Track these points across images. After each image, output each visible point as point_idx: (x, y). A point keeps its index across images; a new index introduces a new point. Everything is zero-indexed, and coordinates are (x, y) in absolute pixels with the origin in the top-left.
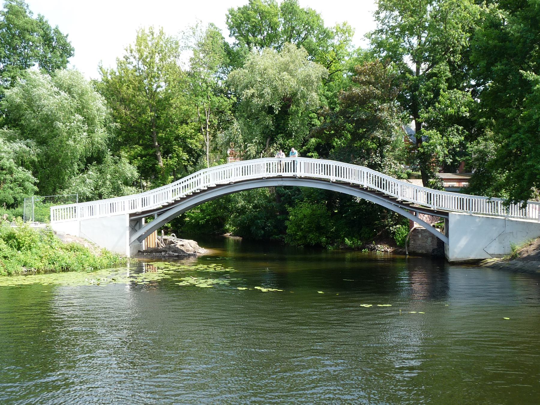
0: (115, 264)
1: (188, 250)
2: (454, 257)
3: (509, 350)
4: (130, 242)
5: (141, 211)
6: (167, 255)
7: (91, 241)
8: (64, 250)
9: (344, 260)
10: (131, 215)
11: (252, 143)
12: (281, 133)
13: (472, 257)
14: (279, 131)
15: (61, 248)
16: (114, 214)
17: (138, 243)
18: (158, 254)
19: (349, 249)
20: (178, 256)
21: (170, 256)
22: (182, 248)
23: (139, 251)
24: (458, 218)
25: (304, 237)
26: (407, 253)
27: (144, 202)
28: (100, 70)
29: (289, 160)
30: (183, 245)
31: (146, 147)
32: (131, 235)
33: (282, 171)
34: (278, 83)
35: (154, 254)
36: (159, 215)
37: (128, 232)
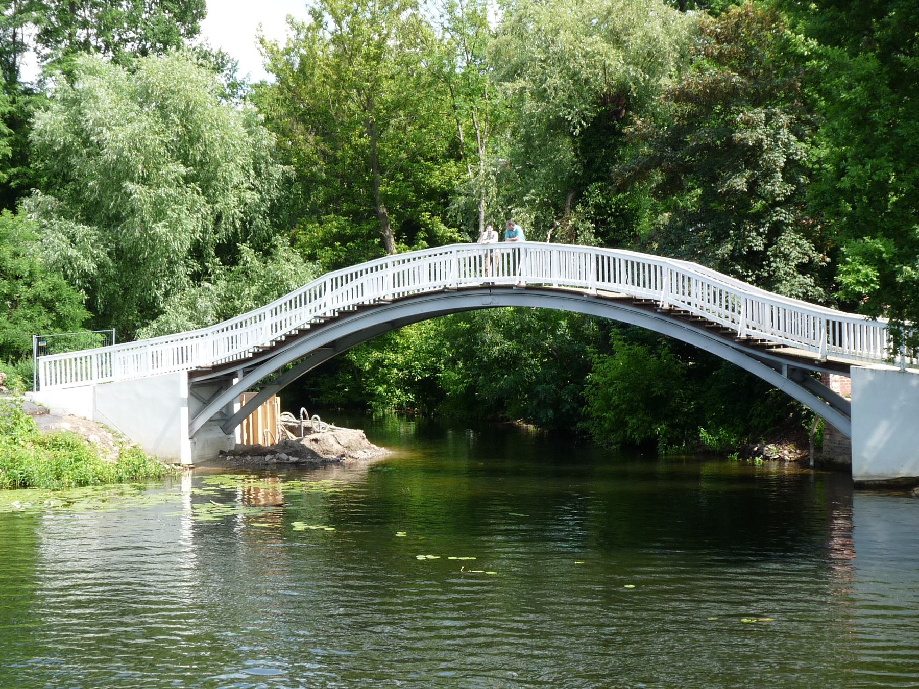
0: (139, 475)
1: (326, 452)
2: (862, 472)
3: (101, 589)
4: (190, 431)
5: (211, 365)
6: (275, 460)
7: (115, 429)
8: (38, 446)
9: (697, 477)
10: (192, 374)
11: (522, 205)
12: (597, 180)
13: (905, 471)
14: (594, 175)
15: (34, 442)
16: (160, 370)
17: (217, 433)
18: (257, 459)
19: (709, 454)
20: (296, 464)
21: (281, 465)
22: (314, 447)
23: (222, 452)
24: (870, 377)
25: (620, 424)
26: (812, 463)
27: (232, 341)
28: (261, 46)
29: (507, 247)
30: (316, 441)
31: (357, 217)
32: (193, 417)
33: (495, 273)
34: (578, 64)
35: (249, 458)
36: (246, 372)
37: (185, 412)
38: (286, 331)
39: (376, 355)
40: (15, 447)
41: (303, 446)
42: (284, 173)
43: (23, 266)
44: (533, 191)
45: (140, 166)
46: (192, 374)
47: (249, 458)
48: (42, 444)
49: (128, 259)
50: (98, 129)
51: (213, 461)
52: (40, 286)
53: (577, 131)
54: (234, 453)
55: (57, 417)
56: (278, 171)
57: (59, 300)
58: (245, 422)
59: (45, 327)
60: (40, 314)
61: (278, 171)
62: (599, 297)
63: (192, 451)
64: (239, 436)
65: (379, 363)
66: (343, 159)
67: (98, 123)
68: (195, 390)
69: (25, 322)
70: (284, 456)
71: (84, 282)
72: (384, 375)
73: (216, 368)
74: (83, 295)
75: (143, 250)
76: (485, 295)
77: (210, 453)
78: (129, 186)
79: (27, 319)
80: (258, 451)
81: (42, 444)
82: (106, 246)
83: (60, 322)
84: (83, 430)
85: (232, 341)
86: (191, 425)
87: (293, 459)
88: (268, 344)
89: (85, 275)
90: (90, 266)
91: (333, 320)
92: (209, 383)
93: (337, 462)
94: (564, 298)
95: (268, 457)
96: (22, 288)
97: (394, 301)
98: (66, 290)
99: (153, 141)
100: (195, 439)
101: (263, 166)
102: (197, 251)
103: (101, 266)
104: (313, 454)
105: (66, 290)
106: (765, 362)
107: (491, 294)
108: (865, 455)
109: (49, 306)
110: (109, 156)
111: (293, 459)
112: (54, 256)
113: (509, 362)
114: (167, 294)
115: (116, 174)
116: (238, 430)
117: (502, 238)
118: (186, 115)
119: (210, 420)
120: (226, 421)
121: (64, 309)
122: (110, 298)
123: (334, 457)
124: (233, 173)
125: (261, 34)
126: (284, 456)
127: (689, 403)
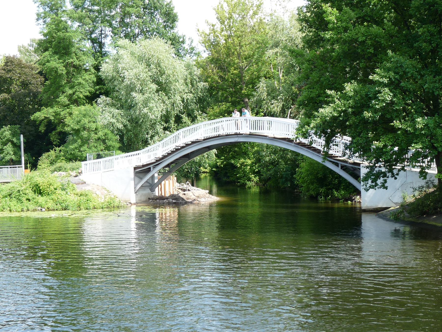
0: (111, 207)
5: (141, 165)
10: (135, 168)
13: (380, 206)
17: (148, 191)
18: (161, 201)
20: (175, 203)
27: (149, 157)
30: (184, 194)
32: (136, 185)
37: (133, 182)
38: (167, 151)
39: (242, 160)
40: (67, 195)
41: (179, 196)
42: (204, 86)
43: (93, 126)
44: (281, 95)
45: (139, 85)
46: (135, 168)
47: (158, 201)
48: (77, 194)
49: (136, 122)
50: (124, 71)
51: (144, 202)
52: (100, 134)
53: (298, 69)
54: (153, 199)
55: (88, 185)
56: (202, 85)
57: (108, 139)
58: (160, 186)
59: (102, 150)
60: (100, 145)
61: (202, 85)
62: (274, 138)
63: (136, 198)
64: (157, 193)
65: (242, 164)
66: (228, 79)
67: (123, 68)
68: (137, 174)
69: (93, 148)
70: (171, 200)
71: (119, 132)
72: (244, 169)
73: (143, 166)
74: (118, 137)
75: (140, 119)
76: (235, 137)
77: (144, 199)
78: (134, 94)
79: (94, 147)
80: (162, 198)
81: (77, 194)
82: (127, 117)
83: (108, 148)
84: (96, 189)
85: (149, 157)
86: (135, 188)
87: (174, 201)
88: (161, 157)
89: (118, 130)
90: (120, 126)
91: (183, 147)
92: (142, 171)
93: (191, 203)
94: (263, 138)
95: (165, 200)
96: (93, 135)
97: (204, 140)
98: (110, 135)
99: (143, 76)
100: (137, 193)
101: (195, 82)
102: (166, 118)
103: (125, 126)
104: (183, 199)
105: (110, 135)
106: (333, 163)
107: (237, 137)
108: (366, 199)
109: (104, 141)
110: (127, 82)
111: (174, 201)
112: (106, 122)
113: (273, 163)
114: (152, 137)
115: (131, 88)
116: (157, 189)
117: (241, 116)
118: (158, 65)
119: (142, 186)
120: (151, 186)
121: (109, 143)
122: (129, 140)
123: (191, 200)
124: (180, 86)
125: (197, 28)
126: (171, 200)
127: (335, 179)
